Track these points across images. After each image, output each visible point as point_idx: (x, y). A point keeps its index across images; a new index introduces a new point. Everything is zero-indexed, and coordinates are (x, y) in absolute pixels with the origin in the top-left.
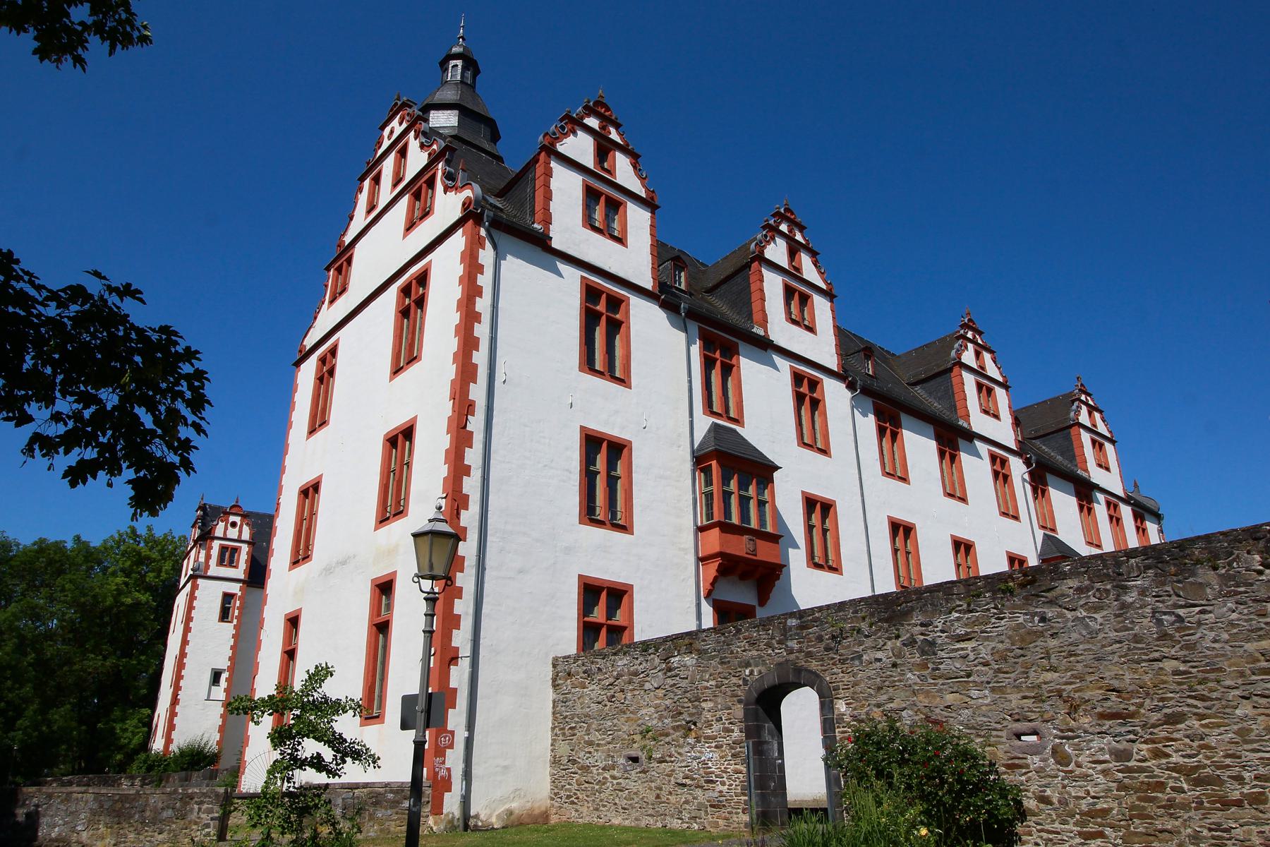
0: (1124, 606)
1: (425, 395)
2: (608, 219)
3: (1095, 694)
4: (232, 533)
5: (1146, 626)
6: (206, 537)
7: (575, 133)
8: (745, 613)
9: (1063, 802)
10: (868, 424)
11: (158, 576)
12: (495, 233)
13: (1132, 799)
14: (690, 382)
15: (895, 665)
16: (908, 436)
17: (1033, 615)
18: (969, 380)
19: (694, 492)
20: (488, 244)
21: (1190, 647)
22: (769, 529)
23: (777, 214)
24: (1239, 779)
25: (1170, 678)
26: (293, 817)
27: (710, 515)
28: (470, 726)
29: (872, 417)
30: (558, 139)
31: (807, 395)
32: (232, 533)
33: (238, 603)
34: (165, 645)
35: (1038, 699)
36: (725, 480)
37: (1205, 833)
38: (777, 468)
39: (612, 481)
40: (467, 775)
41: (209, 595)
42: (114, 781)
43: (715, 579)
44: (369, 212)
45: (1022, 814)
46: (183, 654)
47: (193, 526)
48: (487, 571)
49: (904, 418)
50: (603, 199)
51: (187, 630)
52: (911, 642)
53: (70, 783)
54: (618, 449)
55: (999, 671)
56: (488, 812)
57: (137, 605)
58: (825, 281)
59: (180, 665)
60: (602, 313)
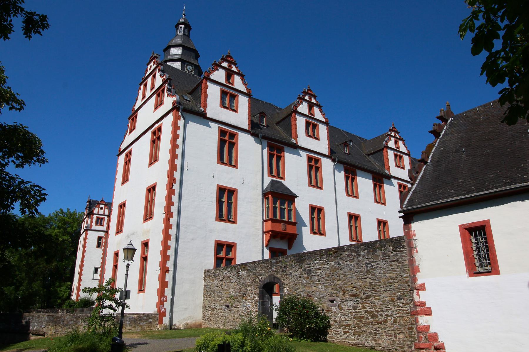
0: (359, 261)
1: (159, 175)
3: (350, 288)
4: (101, 212)
5: (363, 268)
6: (91, 214)
7: (217, 70)
9: (340, 322)
10: (341, 176)
11: (72, 228)
12: (184, 114)
13: (356, 321)
14: (263, 164)
15: (300, 277)
16: (359, 179)
18: (391, 154)
21: (373, 275)
22: (292, 220)
24: (381, 315)
27: (268, 216)
30: (210, 73)
31: (314, 165)
32: (101, 212)
33: (104, 241)
35: (336, 290)
36: (275, 202)
37: (373, 332)
38: (297, 197)
39: (229, 205)
40: (172, 311)
41: (93, 237)
42: (56, 311)
43: (269, 240)
45: (330, 326)
46: (83, 261)
47: (86, 209)
48: (180, 240)
49: (358, 172)
50: (229, 95)
51: (84, 251)
52: (305, 270)
53: (40, 312)
54: (232, 192)
55: (327, 280)
56: (179, 323)
57: (64, 240)
58: (325, 118)
59: (82, 265)
60: (227, 142)
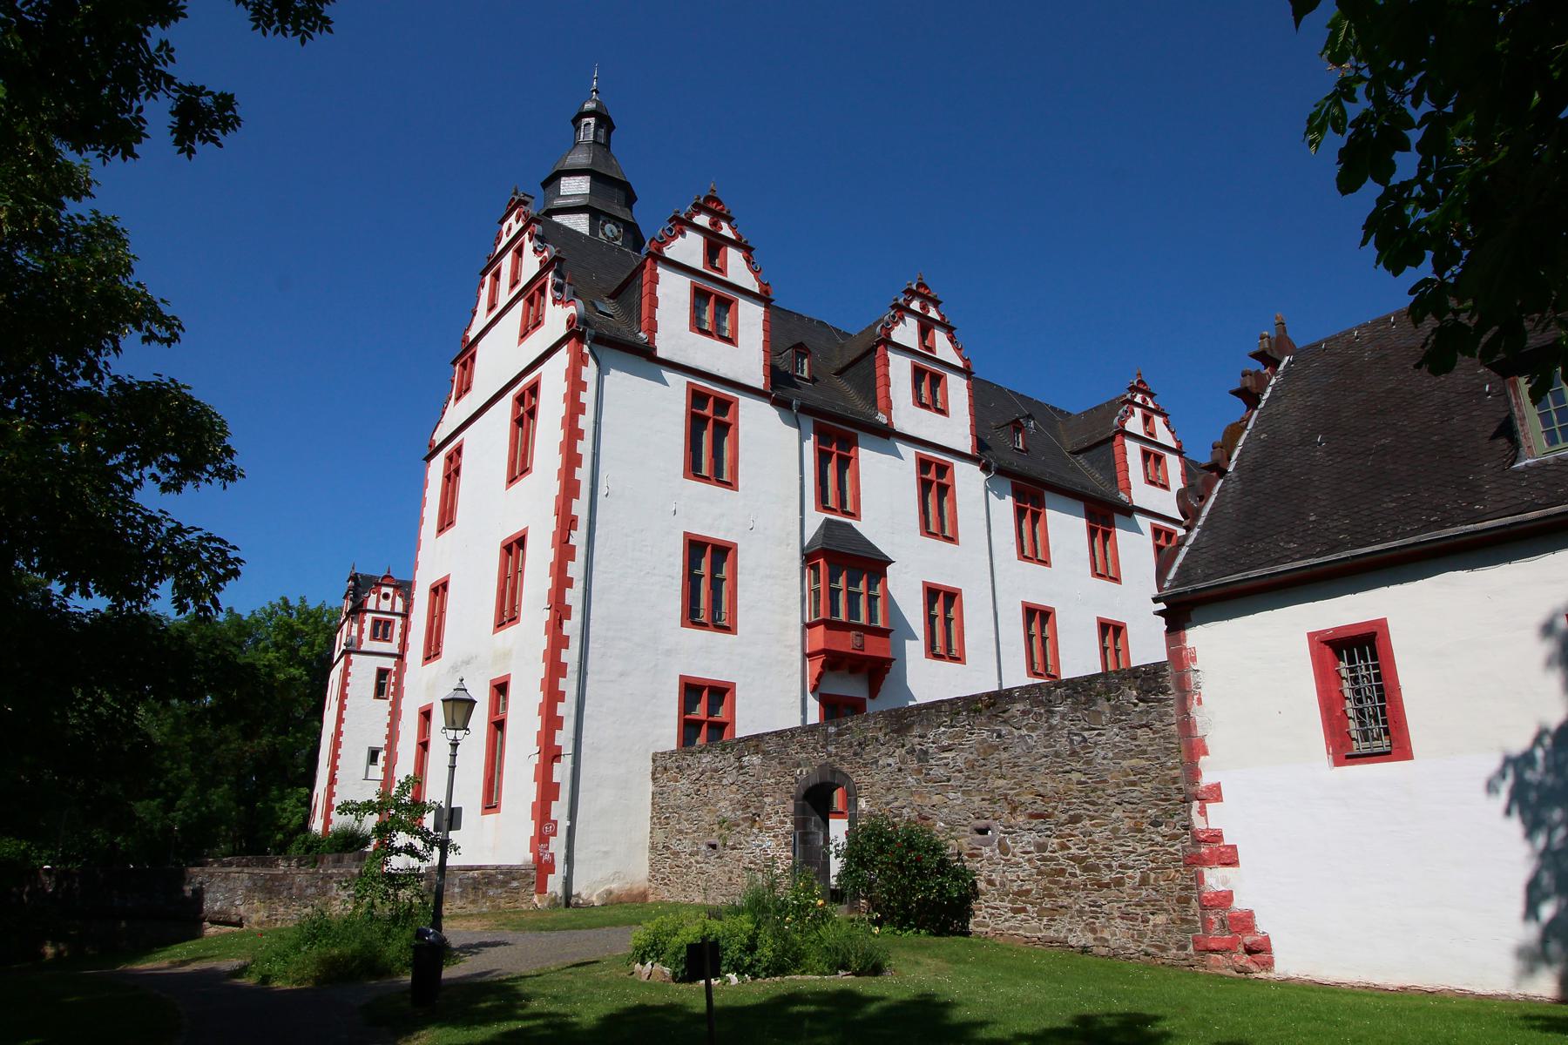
0: (1051, 727)
1: (532, 507)
2: (718, 319)
3: (1027, 798)
5: (1063, 745)
6: (358, 610)
8: (856, 707)
9: (1003, 884)
10: (1005, 507)
12: (599, 350)
14: (802, 479)
15: (900, 770)
16: (1051, 515)
17: (993, 731)
18: (1133, 450)
19: (803, 589)
20: (591, 361)
22: (880, 624)
23: (909, 291)
24: (1109, 866)
25: (1075, 787)
26: (391, 891)
27: (817, 613)
28: (572, 815)
29: (1009, 500)
30: (665, 243)
31: (934, 481)
32: (385, 605)
34: (321, 721)
35: (992, 801)
36: (833, 578)
39: (716, 585)
40: (569, 859)
41: (364, 671)
43: (820, 675)
44: (490, 310)
46: (338, 733)
51: (342, 707)
52: (912, 751)
53: (230, 864)
54: (723, 552)
55: (968, 777)
58: (962, 358)
59: (336, 744)
